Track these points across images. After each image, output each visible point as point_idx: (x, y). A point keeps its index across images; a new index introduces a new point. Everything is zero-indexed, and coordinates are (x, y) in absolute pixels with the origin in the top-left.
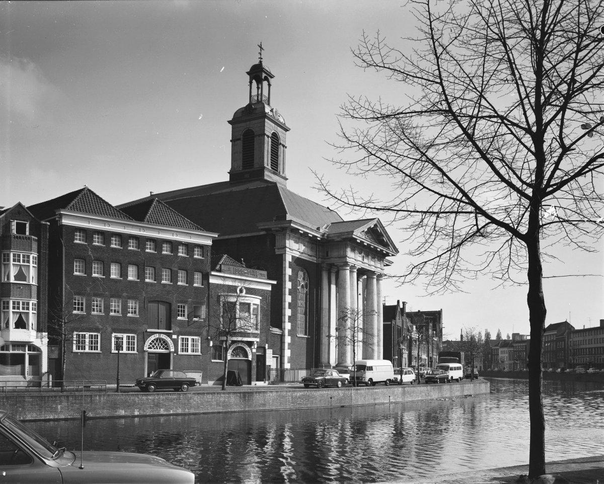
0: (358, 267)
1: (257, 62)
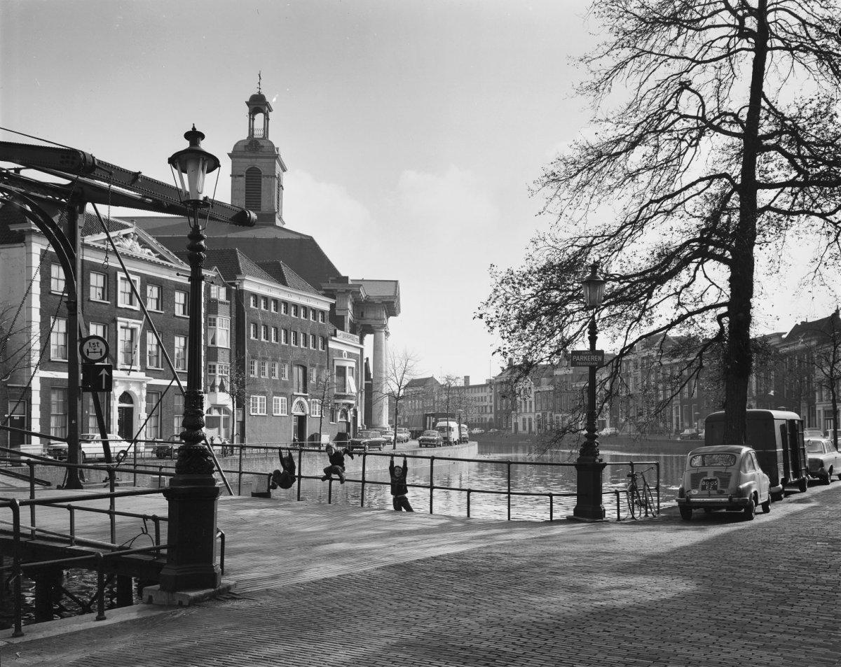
1: (255, 92)
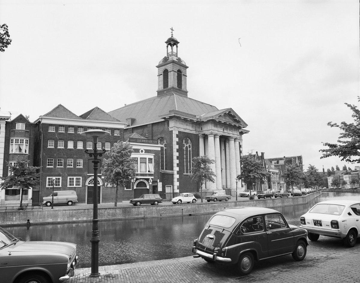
0: (219, 135)
1: (170, 37)
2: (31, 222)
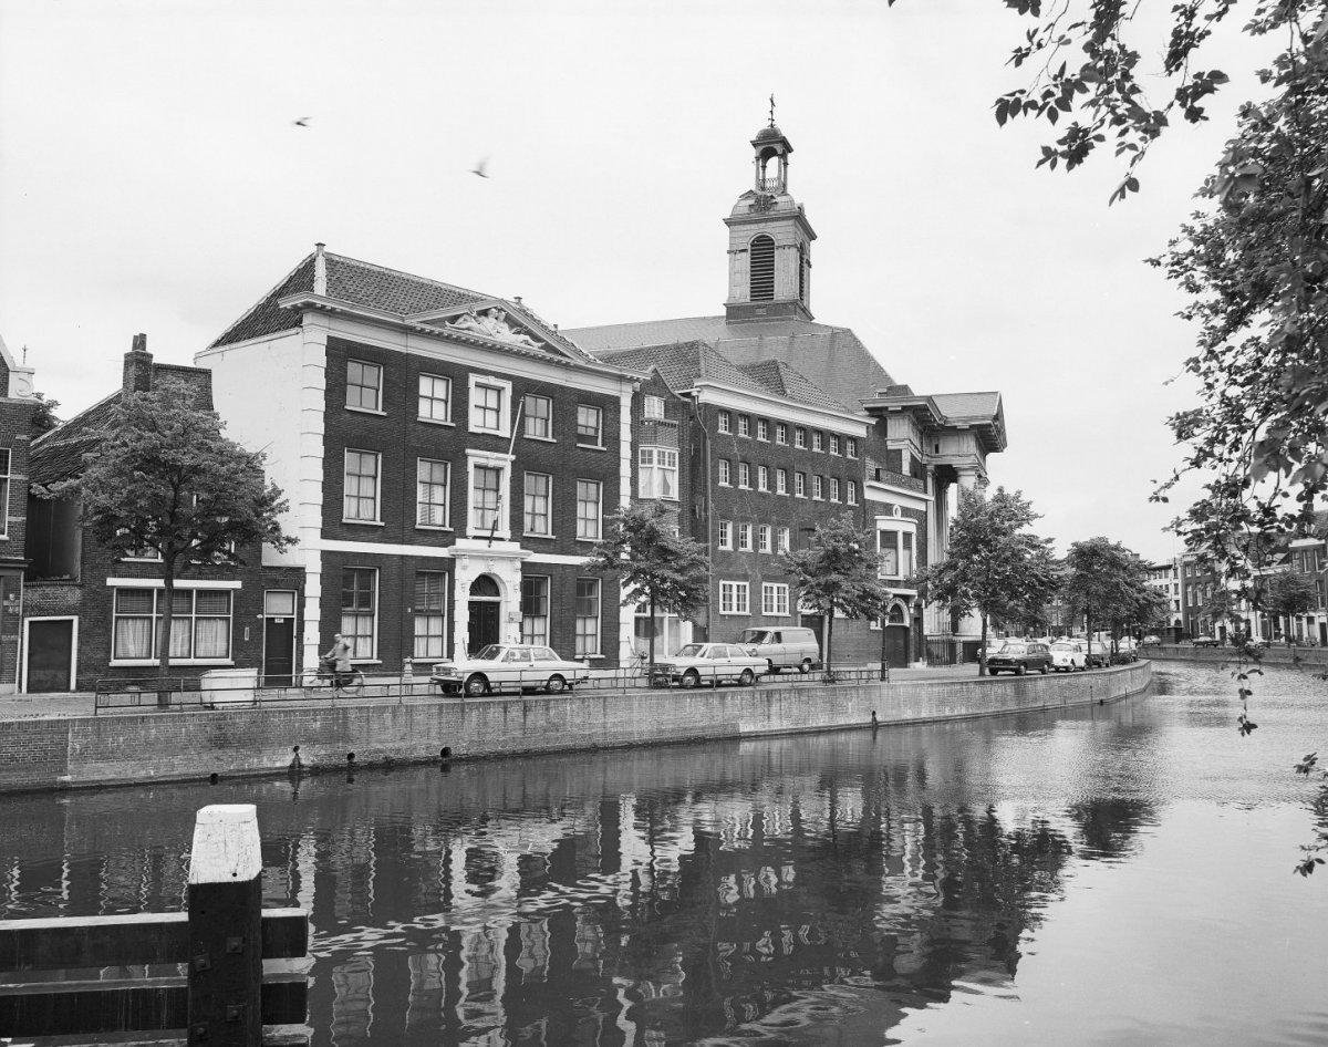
1: (765, 125)
2: (879, 718)
